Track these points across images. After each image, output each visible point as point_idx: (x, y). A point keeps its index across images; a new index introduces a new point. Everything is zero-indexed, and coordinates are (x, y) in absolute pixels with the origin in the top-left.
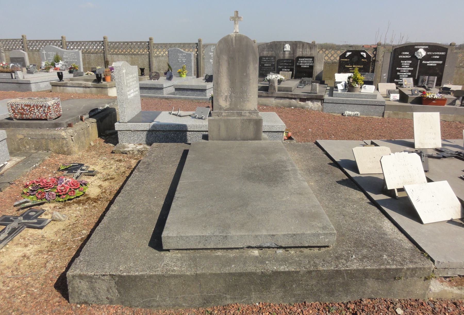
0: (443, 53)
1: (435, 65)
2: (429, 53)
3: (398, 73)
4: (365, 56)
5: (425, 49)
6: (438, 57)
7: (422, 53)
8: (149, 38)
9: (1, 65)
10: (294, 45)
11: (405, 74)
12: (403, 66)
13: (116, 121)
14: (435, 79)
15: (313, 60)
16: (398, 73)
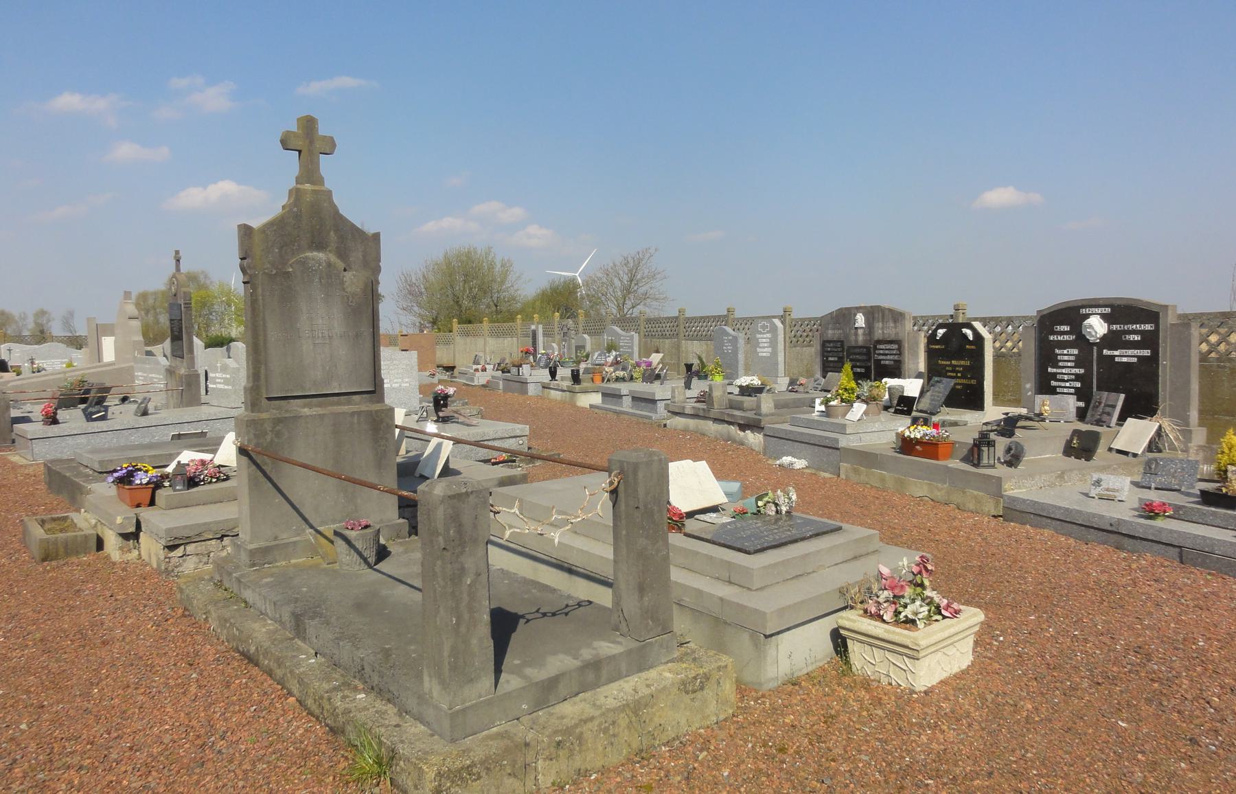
0: (1148, 327)
1: (1135, 360)
2: (1114, 327)
3: (1053, 383)
5: (1104, 317)
6: (1137, 338)
10: (872, 313)
11: (1068, 384)
12: (1061, 364)
15: (899, 349)
16: (1053, 383)
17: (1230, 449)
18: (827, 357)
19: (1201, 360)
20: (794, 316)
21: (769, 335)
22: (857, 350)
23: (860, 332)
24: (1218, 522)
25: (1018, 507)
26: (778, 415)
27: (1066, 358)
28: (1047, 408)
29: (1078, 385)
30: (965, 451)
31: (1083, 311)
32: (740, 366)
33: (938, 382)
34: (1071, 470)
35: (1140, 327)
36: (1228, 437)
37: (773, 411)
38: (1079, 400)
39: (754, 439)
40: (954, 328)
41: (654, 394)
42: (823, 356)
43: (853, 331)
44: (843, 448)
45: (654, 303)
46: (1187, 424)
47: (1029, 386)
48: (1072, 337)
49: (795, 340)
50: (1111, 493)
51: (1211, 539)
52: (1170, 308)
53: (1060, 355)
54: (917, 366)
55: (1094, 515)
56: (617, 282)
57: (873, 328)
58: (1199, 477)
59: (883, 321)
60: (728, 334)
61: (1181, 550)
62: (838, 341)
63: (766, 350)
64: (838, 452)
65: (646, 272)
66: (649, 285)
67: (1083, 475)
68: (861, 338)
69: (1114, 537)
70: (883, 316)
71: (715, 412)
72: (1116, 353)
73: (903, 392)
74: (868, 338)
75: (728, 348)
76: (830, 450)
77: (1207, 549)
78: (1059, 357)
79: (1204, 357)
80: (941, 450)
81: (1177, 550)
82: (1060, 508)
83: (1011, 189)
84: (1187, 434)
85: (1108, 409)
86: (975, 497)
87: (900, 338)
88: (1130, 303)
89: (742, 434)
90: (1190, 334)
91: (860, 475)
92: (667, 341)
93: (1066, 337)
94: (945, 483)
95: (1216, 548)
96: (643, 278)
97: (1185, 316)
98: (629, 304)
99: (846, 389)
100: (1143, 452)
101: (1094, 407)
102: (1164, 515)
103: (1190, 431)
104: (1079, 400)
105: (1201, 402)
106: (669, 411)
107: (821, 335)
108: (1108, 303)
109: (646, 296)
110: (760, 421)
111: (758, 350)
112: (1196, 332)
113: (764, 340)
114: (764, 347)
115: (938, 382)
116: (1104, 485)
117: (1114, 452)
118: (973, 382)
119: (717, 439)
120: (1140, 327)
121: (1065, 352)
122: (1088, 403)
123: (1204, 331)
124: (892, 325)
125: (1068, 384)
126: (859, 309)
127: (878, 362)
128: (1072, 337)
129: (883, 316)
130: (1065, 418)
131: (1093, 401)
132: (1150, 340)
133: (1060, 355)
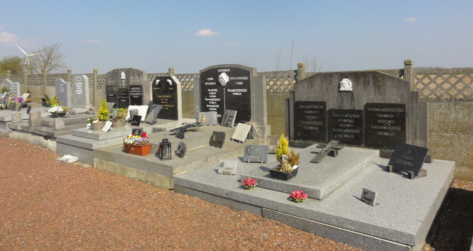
0: (246, 78)
1: (241, 94)
2: (232, 78)
3: (208, 106)
4: (171, 84)
5: (227, 73)
6: (241, 83)
7: (224, 78)
8: (298, 65)
9: (472, 132)
10: (129, 72)
11: (214, 106)
12: (210, 96)
13: (146, 160)
14: (234, 114)
15: (141, 90)
16: (208, 106)
17: (283, 145)
18: (109, 94)
19: (267, 93)
20: (99, 73)
21: (81, 83)
22: (122, 91)
23: (123, 81)
24: (279, 188)
25: (181, 184)
26: (68, 129)
27: (212, 93)
28: (204, 118)
29: (218, 106)
30: (156, 150)
31: (219, 71)
32: (68, 99)
33: (155, 107)
34: (211, 156)
36: (281, 138)
37: (64, 127)
38: (218, 114)
39: (51, 144)
40: (164, 79)
41: (4, 118)
42: (107, 94)
43: (120, 81)
44: (94, 149)
45: (61, 69)
46: (263, 124)
47: (198, 107)
49: (99, 85)
50: (229, 170)
51: (277, 203)
53: (210, 92)
54: (150, 98)
55: (218, 189)
56: (41, 59)
57: (129, 79)
59: (133, 76)
60: (62, 83)
61: (262, 209)
63: (80, 91)
64: (93, 151)
69: (228, 202)
70: (133, 73)
71: (32, 129)
72: (233, 91)
73: (137, 113)
74: (127, 84)
75: (62, 90)
76: (89, 151)
77: (275, 209)
79: (268, 92)
80: (144, 150)
81: (260, 209)
82: (202, 184)
83: (209, 30)
84: (263, 129)
85: (230, 118)
86: (160, 178)
87: (141, 84)
89: (45, 141)
90: (262, 82)
91: (103, 165)
93: (212, 83)
94: (145, 170)
95: (279, 208)
96: (55, 57)
97: (260, 73)
98: (47, 69)
99: (102, 114)
100: (245, 140)
101: (224, 117)
102: (253, 187)
103: (264, 128)
104: (218, 114)
105: (268, 112)
106: (10, 129)
107: (106, 83)
108: (229, 67)
109: (56, 65)
110: (53, 134)
111: (77, 91)
112: (265, 80)
113: (79, 86)
115: (155, 107)
116: (225, 166)
117: (233, 141)
118: (173, 106)
119: (34, 145)
121: (212, 90)
122: (222, 115)
123: (268, 80)
124: (137, 78)
125: (214, 106)
126: (122, 70)
127: (131, 96)
129: (133, 73)
130: (213, 123)
131: (224, 115)
132: (247, 85)
133: (210, 92)
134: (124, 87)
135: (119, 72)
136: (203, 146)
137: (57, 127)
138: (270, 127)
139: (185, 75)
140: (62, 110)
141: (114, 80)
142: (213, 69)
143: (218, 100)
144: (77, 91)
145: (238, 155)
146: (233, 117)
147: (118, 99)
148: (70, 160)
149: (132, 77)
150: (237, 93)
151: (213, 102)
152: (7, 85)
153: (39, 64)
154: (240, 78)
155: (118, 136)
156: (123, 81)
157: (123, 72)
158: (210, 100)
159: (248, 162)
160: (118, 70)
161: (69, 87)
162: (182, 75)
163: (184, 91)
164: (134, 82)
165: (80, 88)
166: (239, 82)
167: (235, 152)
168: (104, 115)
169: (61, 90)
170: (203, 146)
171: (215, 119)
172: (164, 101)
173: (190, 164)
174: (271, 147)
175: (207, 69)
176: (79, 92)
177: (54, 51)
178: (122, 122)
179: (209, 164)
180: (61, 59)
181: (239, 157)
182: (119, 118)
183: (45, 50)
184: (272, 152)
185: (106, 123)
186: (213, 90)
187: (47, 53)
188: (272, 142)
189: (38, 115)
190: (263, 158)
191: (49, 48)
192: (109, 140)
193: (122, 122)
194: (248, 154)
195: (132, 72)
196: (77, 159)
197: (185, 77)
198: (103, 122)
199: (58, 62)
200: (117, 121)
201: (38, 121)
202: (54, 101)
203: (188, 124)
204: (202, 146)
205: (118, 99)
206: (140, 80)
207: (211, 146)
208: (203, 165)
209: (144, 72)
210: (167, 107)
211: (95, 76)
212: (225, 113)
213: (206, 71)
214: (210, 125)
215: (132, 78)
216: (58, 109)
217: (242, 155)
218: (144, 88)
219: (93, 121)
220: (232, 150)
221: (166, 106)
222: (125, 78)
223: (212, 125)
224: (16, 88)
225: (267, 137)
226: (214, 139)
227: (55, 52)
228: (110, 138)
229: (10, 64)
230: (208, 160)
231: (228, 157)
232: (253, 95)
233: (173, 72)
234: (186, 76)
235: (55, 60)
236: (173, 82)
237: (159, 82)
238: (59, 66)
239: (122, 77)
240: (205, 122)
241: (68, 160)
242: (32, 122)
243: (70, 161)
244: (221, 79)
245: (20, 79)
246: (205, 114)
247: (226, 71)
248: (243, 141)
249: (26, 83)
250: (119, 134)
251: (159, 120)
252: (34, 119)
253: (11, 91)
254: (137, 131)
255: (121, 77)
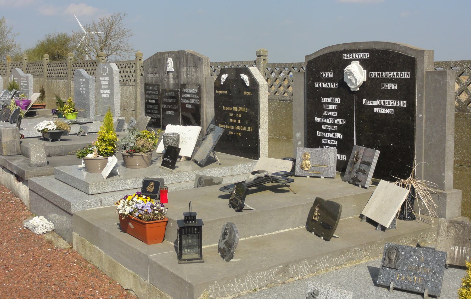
0: (405, 75)
1: (391, 111)
3: (319, 134)
5: (363, 63)
6: (394, 87)
11: (331, 136)
12: (325, 113)
14: (372, 157)
16: (319, 134)
21: (107, 78)
22: (168, 94)
23: (171, 75)
27: (330, 107)
28: (308, 162)
29: (340, 136)
31: (346, 56)
34: (298, 261)
35: (397, 74)
42: (146, 99)
45: (124, 53)
46: (442, 186)
48: (335, 85)
52: (426, 54)
56: (97, 38)
57: (180, 73)
58: (448, 262)
60: (82, 76)
62: (156, 85)
65: (118, 30)
66: (119, 40)
67: (315, 265)
68: (171, 82)
72: (375, 103)
78: (324, 106)
80: (150, 230)
85: (364, 167)
88: (388, 47)
92: (61, 82)
94: (147, 280)
96: (115, 35)
103: (444, 195)
111: (102, 91)
114: (105, 89)
117: (364, 221)
118: (250, 129)
120: (397, 74)
121: (329, 100)
124: (193, 69)
125: (331, 136)
127: (184, 104)
128: (335, 85)
129: (187, 61)
134: (171, 87)
135: (164, 59)
136: (291, 229)
137: (33, 160)
138: (461, 195)
139: (287, 65)
140: (55, 127)
141: (156, 73)
142: (333, 53)
143: (342, 122)
144: (102, 91)
145: (372, 259)
146: (371, 163)
147: (162, 108)
148: (39, 228)
149: (185, 68)
150: (384, 109)
151: (330, 126)
152: (17, 79)
153: (93, 45)
154: (392, 74)
155: (128, 187)
156: (171, 75)
157: (171, 59)
158: (324, 120)
159: (388, 288)
160: (162, 54)
161: (92, 84)
162: (281, 64)
163: (285, 98)
164: (187, 77)
165: (106, 87)
166: (389, 84)
167: (363, 252)
168: (107, 143)
169: (81, 89)
170: (291, 229)
171: (331, 165)
172: (234, 118)
173: (241, 280)
174: (457, 250)
175: (321, 54)
176: (105, 93)
177: (114, 25)
178: (143, 158)
179: (292, 280)
180: (124, 37)
181: (371, 265)
182: (138, 151)
183: (102, 24)
184: (458, 264)
185: (109, 160)
186: (332, 100)
187: (104, 29)
188: (461, 237)
189: (14, 135)
190: (429, 283)
191: (108, 20)
192: (106, 196)
193: (143, 158)
194: (390, 268)
195: (185, 59)
196: (52, 226)
197: (286, 69)
198: (104, 158)
199: (120, 43)
200: (134, 155)
201: (14, 146)
202: (69, 108)
203: (262, 175)
204: (287, 230)
205: (162, 108)
206: (197, 74)
207: (309, 232)
208: (276, 282)
209: (204, 59)
210: (239, 131)
211: (138, 66)
212: (354, 152)
213: (319, 57)
214: (320, 177)
215: (184, 69)
216: (48, 125)
217: (377, 262)
218: (204, 90)
219: (87, 154)
220: (356, 248)
221: (238, 128)
222: (173, 70)
223: (325, 177)
224: (28, 83)
225: (447, 224)
226: (315, 217)
227: (117, 27)
228: (112, 191)
229: (55, 45)
230: (291, 271)
231: (344, 264)
232: (421, 116)
233: (264, 60)
234: (290, 68)
235: (116, 40)
236: (253, 80)
237: (227, 79)
238: (122, 50)
239: (168, 69)
240: (309, 171)
241: (35, 228)
242: (3, 147)
243: (39, 231)
244: (349, 75)
245: (129, 71)
246: (309, 153)
247: (360, 58)
248: (387, 227)
249: (45, 75)
250: (129, 183)
251: (219, 156)
252: (7, 143)
253: (22, 89)
254: (152, 184)
255: (167, 68)
